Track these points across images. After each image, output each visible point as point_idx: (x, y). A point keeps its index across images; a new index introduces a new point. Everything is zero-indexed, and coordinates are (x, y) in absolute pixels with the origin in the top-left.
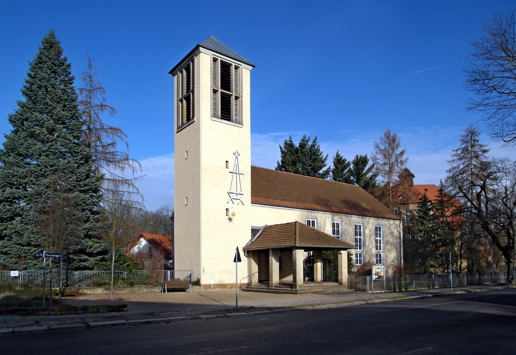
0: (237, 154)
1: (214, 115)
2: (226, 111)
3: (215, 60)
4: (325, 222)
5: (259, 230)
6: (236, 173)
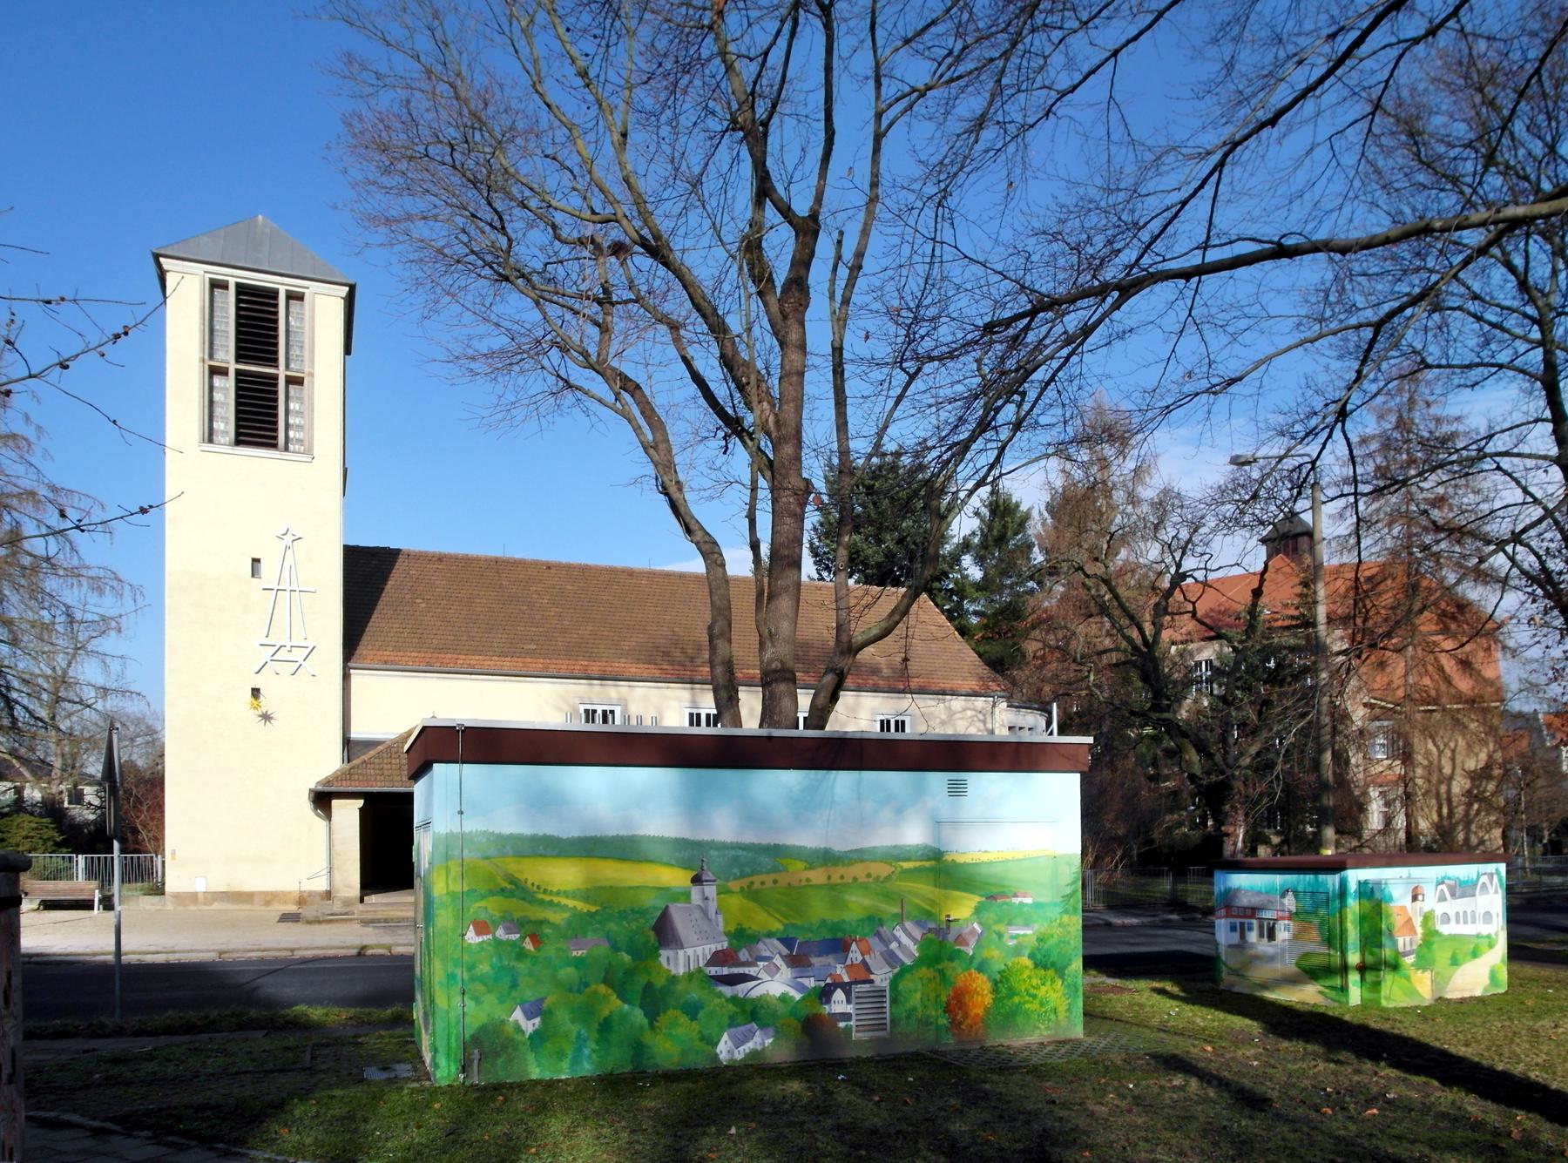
2: (257, 418)
3: (216, 285)
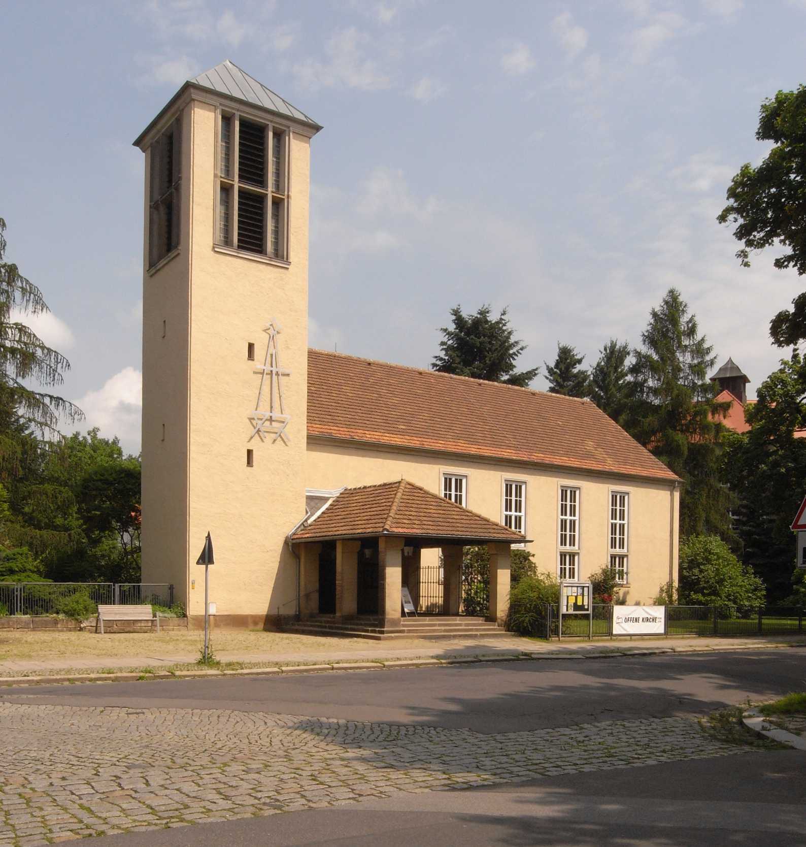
0: (272, 333)
1: (227, 242)
3: (227, 120)
4: (483, 495)
5: (327, 499)
6: (273, 374)
